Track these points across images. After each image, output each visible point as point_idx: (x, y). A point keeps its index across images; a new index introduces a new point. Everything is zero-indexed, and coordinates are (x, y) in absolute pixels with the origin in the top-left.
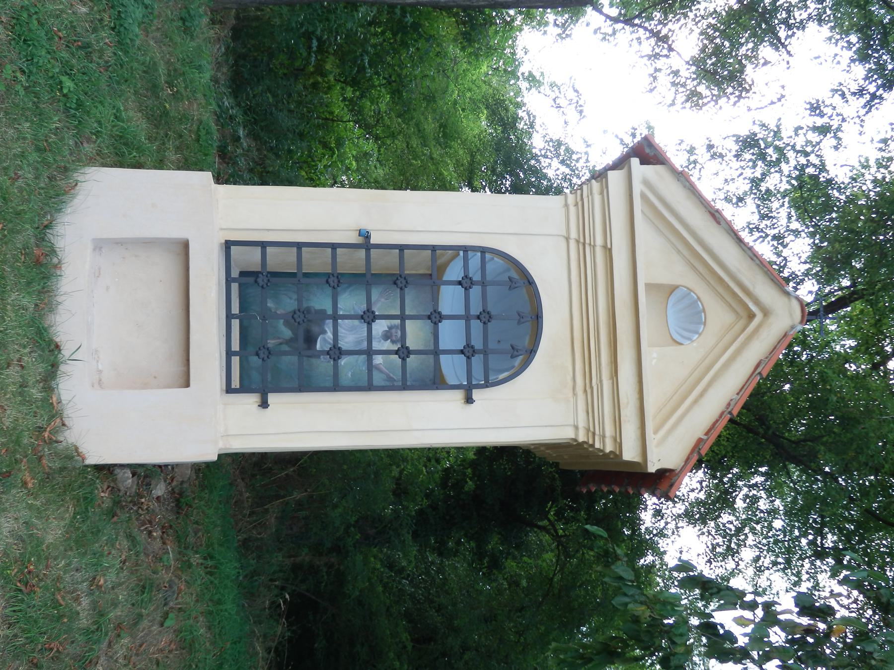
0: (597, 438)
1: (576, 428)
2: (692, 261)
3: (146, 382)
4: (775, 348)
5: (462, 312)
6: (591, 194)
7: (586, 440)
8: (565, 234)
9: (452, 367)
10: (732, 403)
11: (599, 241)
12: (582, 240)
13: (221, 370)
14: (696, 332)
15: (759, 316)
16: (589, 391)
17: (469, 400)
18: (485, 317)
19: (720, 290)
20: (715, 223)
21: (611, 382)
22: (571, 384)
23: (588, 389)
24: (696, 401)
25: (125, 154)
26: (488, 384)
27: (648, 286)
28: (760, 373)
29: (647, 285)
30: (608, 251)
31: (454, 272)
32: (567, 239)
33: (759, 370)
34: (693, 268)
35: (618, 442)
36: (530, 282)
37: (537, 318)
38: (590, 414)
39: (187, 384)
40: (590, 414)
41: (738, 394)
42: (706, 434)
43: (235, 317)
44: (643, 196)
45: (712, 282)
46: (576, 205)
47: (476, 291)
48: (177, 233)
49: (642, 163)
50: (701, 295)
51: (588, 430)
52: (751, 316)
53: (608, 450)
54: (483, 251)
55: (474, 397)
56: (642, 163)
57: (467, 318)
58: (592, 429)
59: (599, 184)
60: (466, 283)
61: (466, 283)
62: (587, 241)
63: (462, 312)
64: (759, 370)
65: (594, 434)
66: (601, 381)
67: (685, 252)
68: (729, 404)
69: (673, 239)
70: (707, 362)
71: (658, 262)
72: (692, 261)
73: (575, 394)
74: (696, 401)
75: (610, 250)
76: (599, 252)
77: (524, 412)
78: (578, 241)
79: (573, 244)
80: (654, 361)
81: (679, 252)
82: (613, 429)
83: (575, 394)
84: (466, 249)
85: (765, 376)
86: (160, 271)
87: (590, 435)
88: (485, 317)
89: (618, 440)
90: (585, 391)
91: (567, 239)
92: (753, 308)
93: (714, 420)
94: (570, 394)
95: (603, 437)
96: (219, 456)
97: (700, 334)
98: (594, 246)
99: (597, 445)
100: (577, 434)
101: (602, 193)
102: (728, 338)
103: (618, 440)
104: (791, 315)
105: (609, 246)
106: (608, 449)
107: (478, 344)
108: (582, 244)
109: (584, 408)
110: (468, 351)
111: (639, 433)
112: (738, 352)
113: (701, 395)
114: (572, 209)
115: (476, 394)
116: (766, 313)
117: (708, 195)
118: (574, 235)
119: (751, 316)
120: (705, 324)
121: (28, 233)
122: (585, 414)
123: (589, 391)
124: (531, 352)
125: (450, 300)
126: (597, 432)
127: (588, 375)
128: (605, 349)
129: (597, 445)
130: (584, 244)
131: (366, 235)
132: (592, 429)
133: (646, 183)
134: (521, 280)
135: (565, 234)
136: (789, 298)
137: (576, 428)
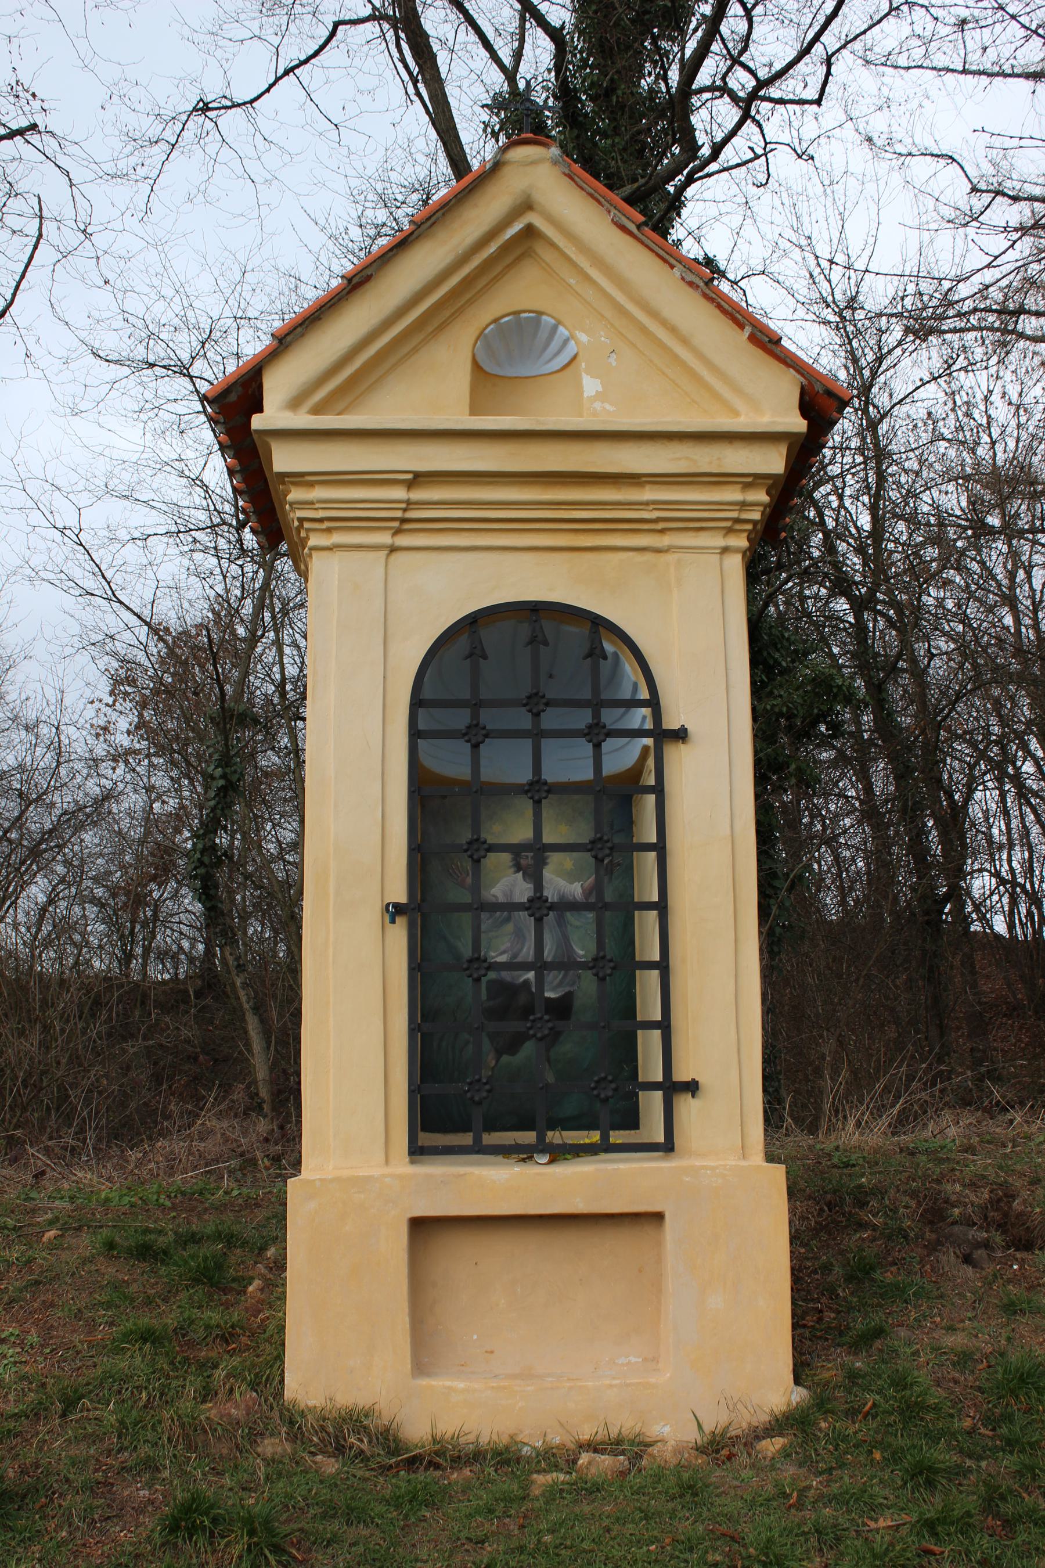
0: (745, 516)
1: (725, 550)
2: (430, 329)
4: (591, 195)
5: (527, 744)
6: (312, 503)
7: (745, 535)
8: (383, 554)
9: (621, 756)
10: (690, 277)
11: (399, 493)
12: (396, 524)
13: (621, 1161)
14: (554, 329)
15: (532, 218)
16: (661, 526)
18: (536, 702)
20: (367, 286)
21: (648, 487)
22: (648, 557)
23: (659, 526)
24: (685, 341)
25: (260, 1345)
26: (654, 702)
27: (473, 412)
28: (639, 227)
29: (473, 412)
30: (418, 479)
31: (451, 761)
32: (393, 549)
33: (633, 228)
35: (753, 480)
36: (473, 622)
39: (658, 1217)
41: (672, 267)
42: (741, 327)
43: (477, 1140)
44: (316, 411)
45: (468, 296)
47: (489, 718)
48: (395, 1243)
49: (260, 410)
50: (488, 317)
51: (729, 531)
52: (530, 231)
53: (765, 498)
54: (417, 702)
55: (677, 727)
56: (260, 410)
57: (537, 735)
58: (728, 524)
59: (312, 536)
60: (476, 736)
61: (476, 736)
62: (399, 514)
63: (527, 744)
64: (633, 228)
65: (737, 521)
66: (647, 503)
68: (691, 284)
69: (393, 359)
71: (434, 391)
72: (430, 329)
74: (685, 341)
76: (417, 495)
77: (691, 634)
78: (397, 532)
79: (402, 541)
80: (608, 406)
82: (730, 487)
84: (415, 734)
85: (642, 219)
86: (461, 1261)
87: (738, 527)
88: (536, 702)
89: (750, 479)
90: (662, 531)
91: (393, 549)
92: (517, 227)
93: (717, 311)
95: (743, 505)
96: (770, 1158)
97: (560, 322)
98: (408, 502)
99: (756, 516)
100: (736, 550)
101: (311, 485)
102: (589, 293)
103: (750, 479)
104: (533, 163)
105: (410, 476)
106: (762, 496)
107: (582, 718)
108: (402, 525)
109: (691, 534)
110: (597, 734)
112: (584, 248)
113: (673, 330)
114: (337, 538)
115: (671, 722)
116: (526, 205)
119: (530, 231)
120: (540, 313)
121: (296, 1005)
122: (703, 534)
123: (661, 526)
124: (597, 624)
125: (507, 763)
126: (735, 515)
127: (634, 526)
128: (587, 489)
129: (756, 516)
130: (404, 521)
132: (728, 524)
133: (295, 404)
134: (471, 636)
135: (383, 554)
136: (504, 163)
137: (725, 550)
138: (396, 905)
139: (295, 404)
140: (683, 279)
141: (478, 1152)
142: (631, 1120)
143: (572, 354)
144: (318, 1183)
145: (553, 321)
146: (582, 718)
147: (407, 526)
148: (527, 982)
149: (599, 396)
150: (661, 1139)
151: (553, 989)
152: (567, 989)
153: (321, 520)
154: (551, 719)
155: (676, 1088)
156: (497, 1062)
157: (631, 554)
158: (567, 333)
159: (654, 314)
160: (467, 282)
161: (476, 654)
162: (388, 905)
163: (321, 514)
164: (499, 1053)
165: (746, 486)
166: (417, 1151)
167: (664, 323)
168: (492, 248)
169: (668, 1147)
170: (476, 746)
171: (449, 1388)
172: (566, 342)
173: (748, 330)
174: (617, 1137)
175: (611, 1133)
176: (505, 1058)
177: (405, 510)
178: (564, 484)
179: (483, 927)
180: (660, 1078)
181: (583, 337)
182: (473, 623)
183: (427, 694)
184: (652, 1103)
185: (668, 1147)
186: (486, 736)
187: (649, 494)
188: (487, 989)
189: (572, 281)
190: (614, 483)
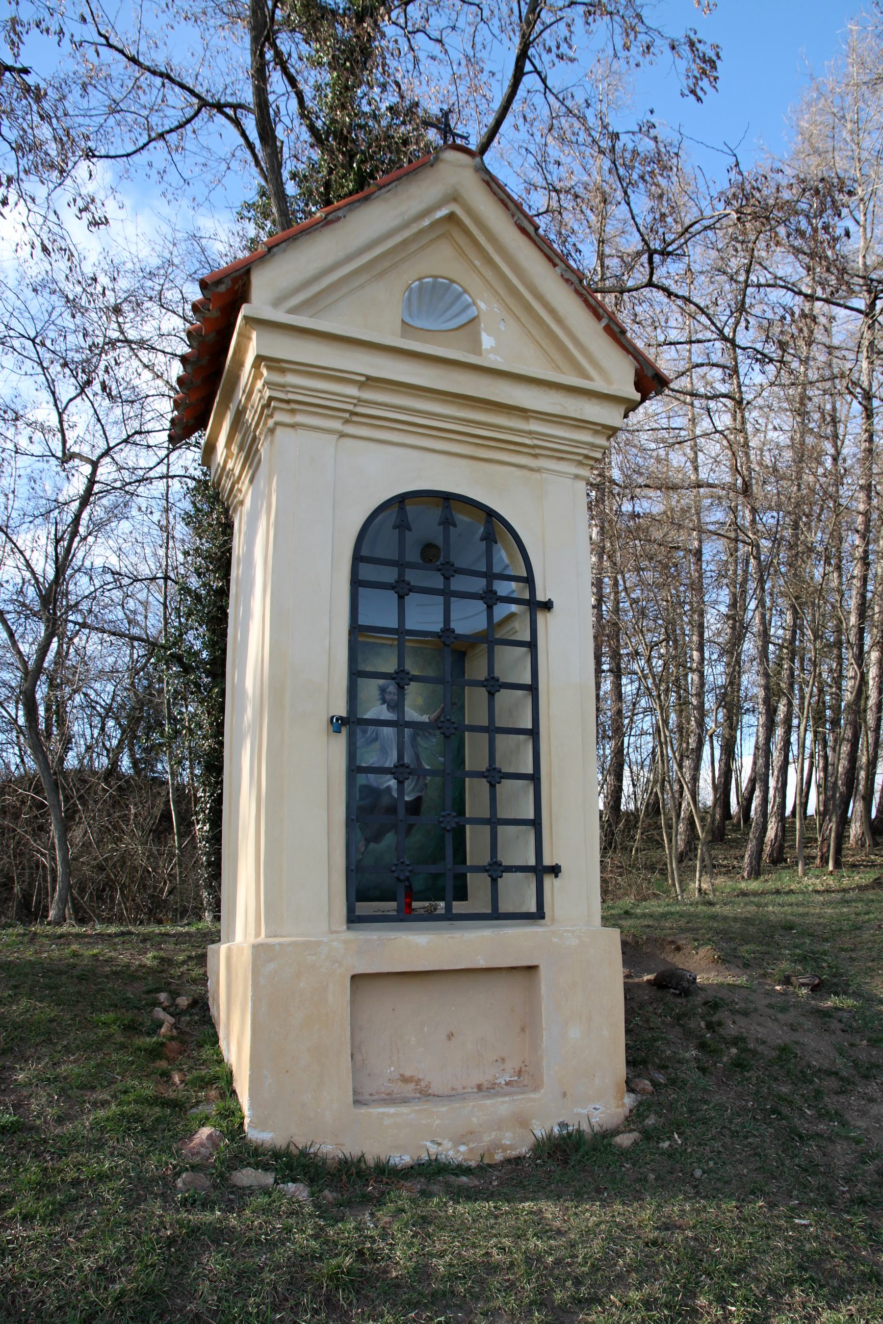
1: (577, 477)
3: (529, 1025)
6: (284, 386)
8: (336, 437)
11: (352, 391)
12: (347, 415)
13: (525, 925)
16: (538, 451)
17: (547, 606)
19: (413, 247)
20: (336, 225)
21: (531, 421)
22: (525, 472)
23: (535, 452)
24: (559, 321)
26: (529, 580)
30: (370, 382)
32: (342, 435)
34: (381, 275)
36: (401, 500)
37: (447, 499)
38: (564, 456)
39: (532, 969)
40: (564, 456)
41: (555, 265)
42: (599, 318)
43: (448, 908)
44: (291, 311)
46: (293, 411)
47: (413, 577)
48: (339, 996)
50: (416, 276)
51: (580, 463)
52: (451, 217)
54: (358, 558)
57: (447, 594)
58: (580, 458)
60: (402, 590)
65: (587, 457)
66: (530, 432)
67: (363, 279)
68: (567, 281)
70: (502, 291)
73: (538, 470)
74: (559, 321)
75: (369, 378)
78: (347, 422)
79: (350, 429)
81: (362, 286)
82: (587, 432)
83: (538, 470)
84: (356, 583)
89: (599, 428)
90: (535, 456)
91: (342, 435)
93: (583, 305)
94: (537, 475)
95: (593, 446)
96: (607, 921)
98: (359, 400)
101: (283, 371)
102: (489, 274)
103: (599, 428)
104: (461, 166)
105: (363, 379)
107: (478, 585)
109: (554, 461)
111: (594, 401)
113: (552, 311)
114: (299, 418)
115: (540, 597)
117: (515, 188)
118: (337, 425)
120: (452, 281)
123: (538, 451)
124: (491, 514)
126: (585, 452)
130: (353, 414)
131: (337, 724)
132: (580, 458)
133: (277, 303)
135: (336, 437)
138: (339, 718)
139: (277, 303)
140: (562, 276)
141: (450, 920)
142: (462, 894)
143: (472, 317)
144: (277, 948)
145: (460, 289)
146: (478, 585)
147: (355, 419)
148: (389, 788)
149: (492, 350)
150: (533, 909)
151: (409, 794)
152: (417, 794)
153: (288, 402)
154: (459, 583)
155: (544, 871)
156: (366, 847)
157: (513, 469)
158: (470, 300)
159: (540, 298)
160: (405, 243)
161: (403, 526)
162: (332, 718)
163: (291, 396)
164: (368, 841)
165: (596, 432)
166: (353, 919)
167: (547, 306)
168: (426, 222)
169: (539, 915)
170: (401, 598)
171: (383, 1113)
172: (468, 306)
173: (605, 322)
174: (458, 907)
175: (454, 903)
176: (372, 845)
177: (355, 405)
178: (473, 407)
179: (358, 744)
180: (532, 862)
181: (482, 305)
182: (400, 502)
183: (364, 552)
184: (477, 883)
185: (539, 915)
186: (410, 590)
187: (534, 426)
188: (360, 792)
189: (477, 263)
190: (508, 413)
